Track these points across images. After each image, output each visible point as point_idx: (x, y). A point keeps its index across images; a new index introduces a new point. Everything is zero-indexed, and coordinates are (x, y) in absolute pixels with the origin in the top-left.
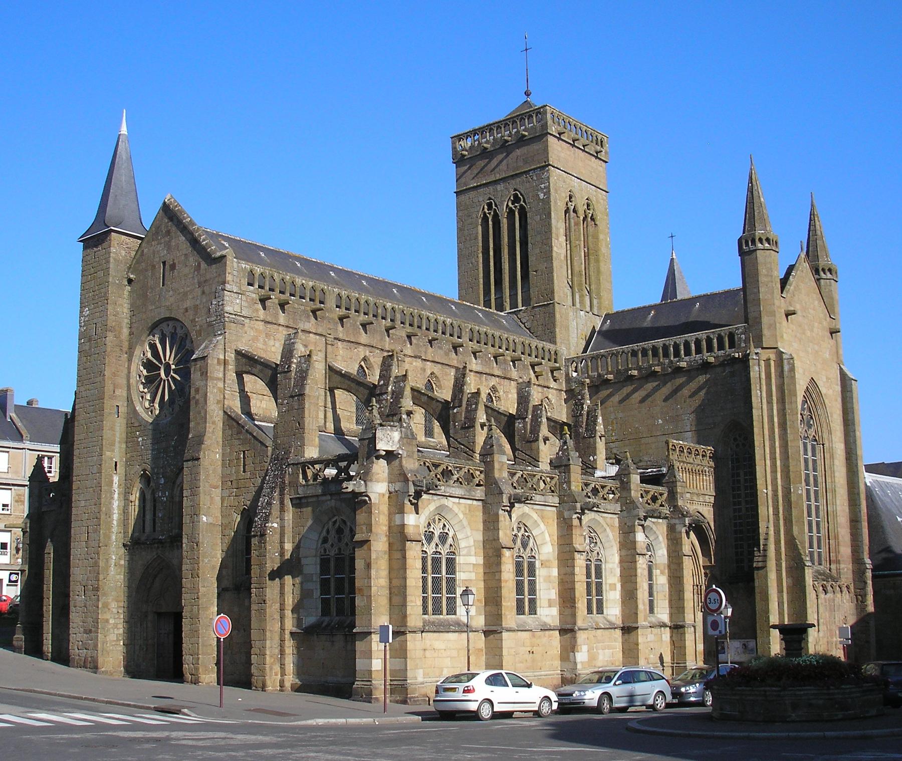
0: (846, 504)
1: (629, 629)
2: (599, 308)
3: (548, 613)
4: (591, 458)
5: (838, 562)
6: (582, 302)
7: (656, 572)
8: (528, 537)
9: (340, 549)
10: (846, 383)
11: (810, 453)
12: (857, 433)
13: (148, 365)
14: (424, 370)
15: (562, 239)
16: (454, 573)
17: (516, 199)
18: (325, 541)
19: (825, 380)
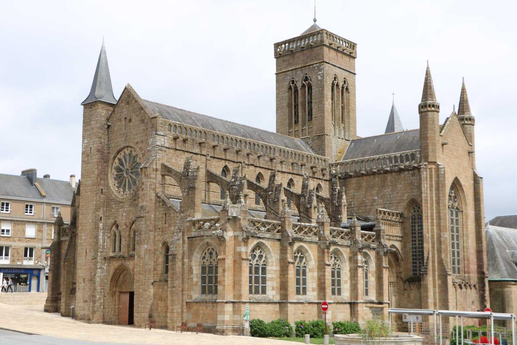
0: (475, 242)
1: (353, 305)
2: (349, 136)
3: (312, 295)
4: (339, 216)
5: (469, 272)
6: (340, 133)
7: (369, 275)
8: (303, 257)
9: (211, 262)
10: (476, 180)
11: (454, 216)
12: (482, 206)
13: (119, 170)
14: (255, 171)
15: (330, 101)
16: (265, 274)
17: (306, 79)
18: (204, 258)
19: (464, 178)
